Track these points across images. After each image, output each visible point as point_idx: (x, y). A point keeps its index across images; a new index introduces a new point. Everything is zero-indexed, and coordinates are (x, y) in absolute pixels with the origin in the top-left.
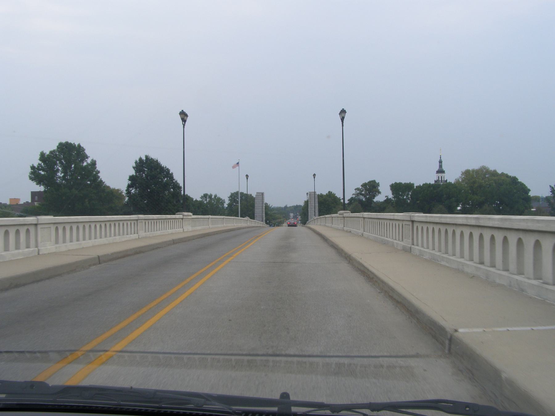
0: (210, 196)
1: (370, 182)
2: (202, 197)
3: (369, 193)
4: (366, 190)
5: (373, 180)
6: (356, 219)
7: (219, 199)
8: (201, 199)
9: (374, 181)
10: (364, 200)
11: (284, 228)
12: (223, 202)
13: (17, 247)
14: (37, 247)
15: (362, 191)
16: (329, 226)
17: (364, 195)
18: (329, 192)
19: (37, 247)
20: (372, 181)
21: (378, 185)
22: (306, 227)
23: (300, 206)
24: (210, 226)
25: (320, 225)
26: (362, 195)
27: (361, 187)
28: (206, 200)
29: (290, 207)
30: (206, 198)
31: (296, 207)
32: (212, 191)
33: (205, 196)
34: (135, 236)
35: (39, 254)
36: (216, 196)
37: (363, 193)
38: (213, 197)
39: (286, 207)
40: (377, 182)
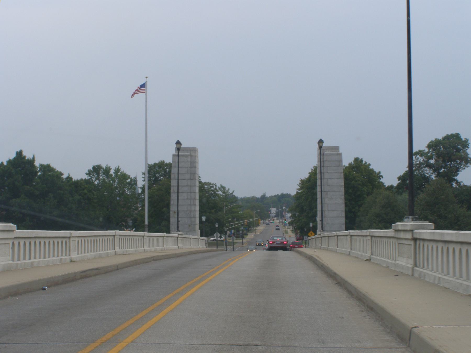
0: (107, 171)
1: (447, 138)
2: (89, 173)
3: (444, 161)
4: (439, 155)
5: (454, 132)
6: (360, 238)
7: (125, 176)
8: (86, 177)
9: (457, 136)
10: (433, 177)
11: (246, 261)
12: (134, 182)
13: (24, 259)
14: (114, 250)
15: (431, 158)
16: (345, 253)
17: (436, 169)
18: (356, 160)
19: (114, 250)
20: (452, 136)
21: (465, 144)
22: (301, 253)
23: (288, 195)
24: (74, 256)
25: (315, 248)
26: (430, 166)
27: (427, 150)
28: (98, 178)
29: (271, 197)
30: (98, 174)
31: (281, 199)
32: (111, 161)
33: (96, 169)
34: (141, 249)
35: (413, 275)
36: (117, 170)
37: (432, 161)
38: (112, 172)
39: (264, 197)
40: (463, 137)
